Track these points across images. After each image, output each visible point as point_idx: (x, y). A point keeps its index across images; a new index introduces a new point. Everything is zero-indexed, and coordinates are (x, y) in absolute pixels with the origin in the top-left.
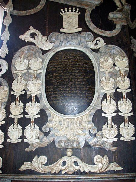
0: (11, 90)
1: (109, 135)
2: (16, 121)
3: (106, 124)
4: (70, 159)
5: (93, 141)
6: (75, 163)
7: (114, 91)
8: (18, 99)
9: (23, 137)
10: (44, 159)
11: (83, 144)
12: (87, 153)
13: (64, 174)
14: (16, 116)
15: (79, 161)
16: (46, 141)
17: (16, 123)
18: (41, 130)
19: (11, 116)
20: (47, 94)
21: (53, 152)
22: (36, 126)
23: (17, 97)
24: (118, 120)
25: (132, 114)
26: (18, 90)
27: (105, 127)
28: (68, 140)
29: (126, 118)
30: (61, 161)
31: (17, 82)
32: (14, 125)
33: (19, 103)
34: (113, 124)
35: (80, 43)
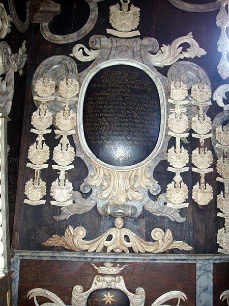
1: (176, 197)
3: (57, 180)
4: (118, 233)
5: (153, 207)
6: (127, 237)
7: (187, 135)
9: (48, 197)
10: (82, 232)
11: (139, 211)
12: (146, 222)
15: (132, 235)
16: (89, 204)
18: (76, 188)
21: (96, 222)
22: (207, 184)
24: (191, 178)
25: (72, 167)
27: (170, 186)
28: (117, 206)
29: (203, 175)
30: (105, 237)
31: (64, 116)
32: (34, 179)
34: (67, 181)
35: (6, 64)
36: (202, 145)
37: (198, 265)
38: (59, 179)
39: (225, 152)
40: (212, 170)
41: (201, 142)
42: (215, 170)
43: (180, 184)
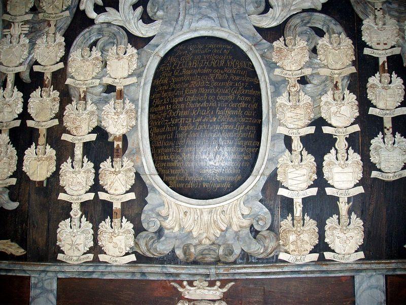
0: (359, 45)
2: (388, 124)
3: (333, 151)
8: (384, 67)
13: (230, 281)
14: (388, 112)
17: (388, 130)
19: (372, 111)
20: (162, 68)
23: (381, 63)
25: (356, 128)
26: (382, 44)
29: (43, 132)
32: (37, 145)
33: (391, 77)
36: (46, 82)
37: (33, 281)
38: (336, 149)
39: (81, 91)
40: (56, 122)
41: (45, 78)
42: (61, 122)
43: (347, 152)
